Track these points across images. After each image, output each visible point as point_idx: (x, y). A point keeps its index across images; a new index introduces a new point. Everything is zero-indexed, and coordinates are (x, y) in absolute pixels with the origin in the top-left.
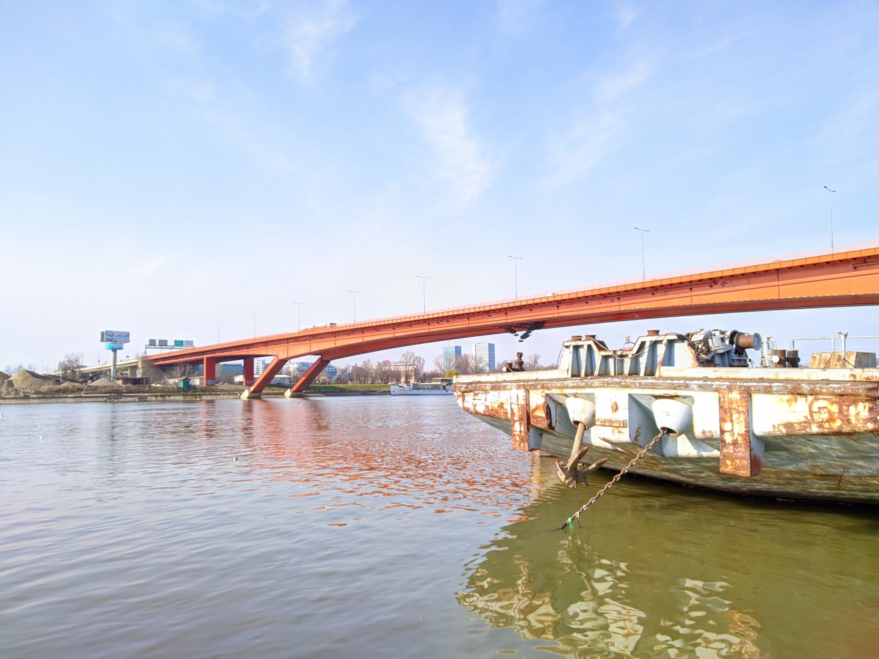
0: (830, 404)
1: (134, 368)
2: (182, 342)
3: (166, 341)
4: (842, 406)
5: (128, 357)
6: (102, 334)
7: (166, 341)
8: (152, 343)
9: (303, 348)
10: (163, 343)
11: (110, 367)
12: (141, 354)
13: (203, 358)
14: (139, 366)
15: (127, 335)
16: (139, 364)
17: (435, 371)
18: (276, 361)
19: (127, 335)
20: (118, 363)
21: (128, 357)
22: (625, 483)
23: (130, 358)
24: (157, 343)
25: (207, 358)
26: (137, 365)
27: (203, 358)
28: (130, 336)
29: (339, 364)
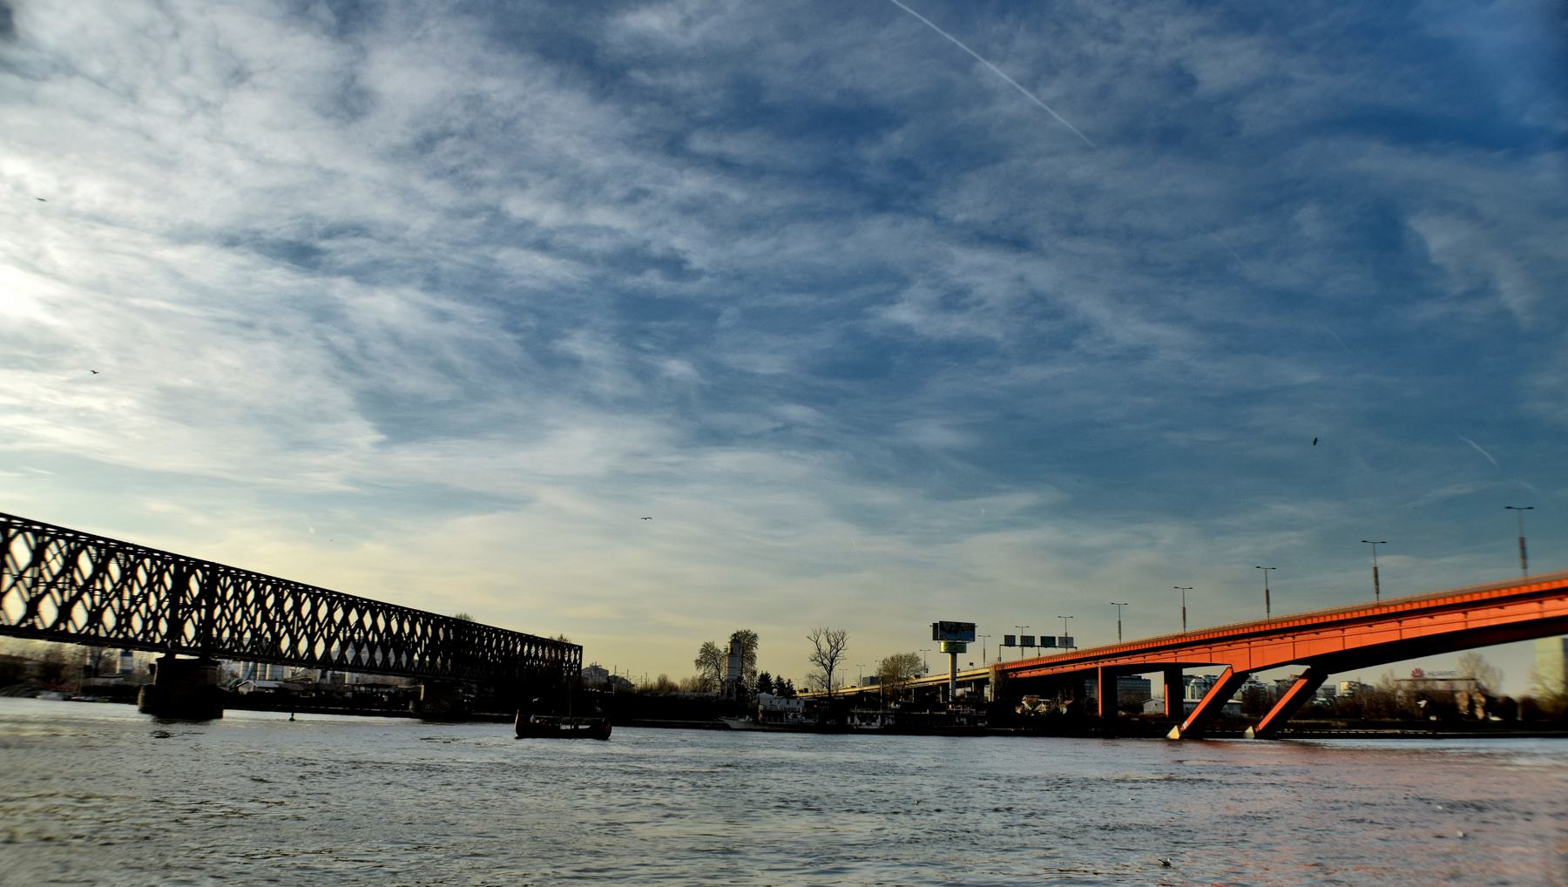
0: (918, 659)
1: (981, 683)
2: (1054, 638)
3: (1032, 638)
4: (87, 591)
5: (971, 664)
6: (935, 625)
7: (1032, 638)
8: (1010, 641)
9: (1282, 649)
10: (1028, 641)
11: (948, 679)
12: (992, 659)
13: (1097, 668)
14: (990, 680)
15: (971, 627)
16: (990, 675)
17: (660, 680)
18: (1229, 674)
19: (971, 627)
20: (958, 675)
21: (971, 664)
22: (287, 268)
23: (975, 666)
24: (1018, 641)
25: (1103, 669)
26: (988, 679)
27: (1097, 668)
28: (976, 629)
29: (1340, 683)
